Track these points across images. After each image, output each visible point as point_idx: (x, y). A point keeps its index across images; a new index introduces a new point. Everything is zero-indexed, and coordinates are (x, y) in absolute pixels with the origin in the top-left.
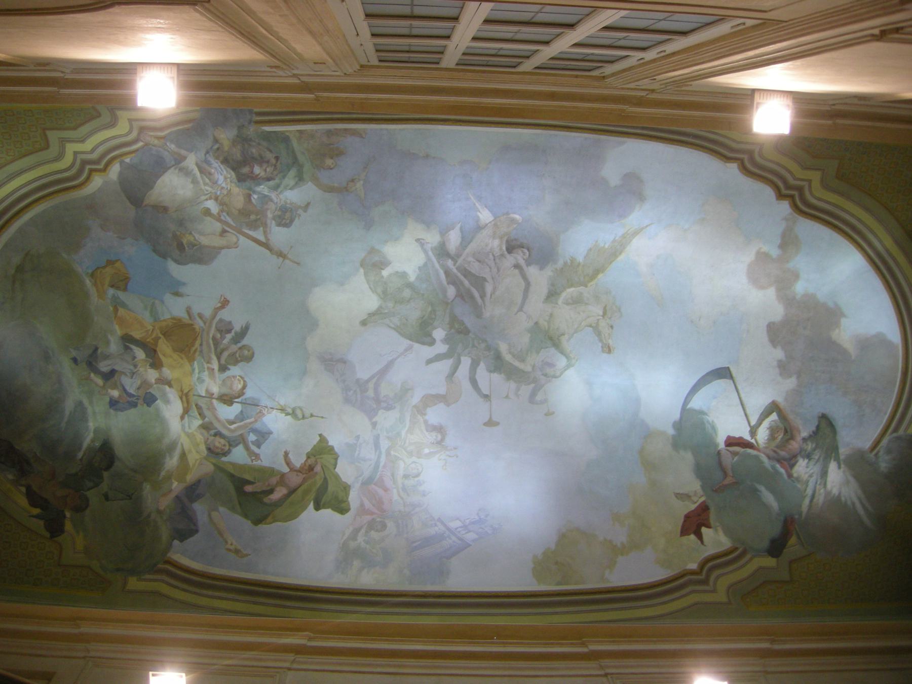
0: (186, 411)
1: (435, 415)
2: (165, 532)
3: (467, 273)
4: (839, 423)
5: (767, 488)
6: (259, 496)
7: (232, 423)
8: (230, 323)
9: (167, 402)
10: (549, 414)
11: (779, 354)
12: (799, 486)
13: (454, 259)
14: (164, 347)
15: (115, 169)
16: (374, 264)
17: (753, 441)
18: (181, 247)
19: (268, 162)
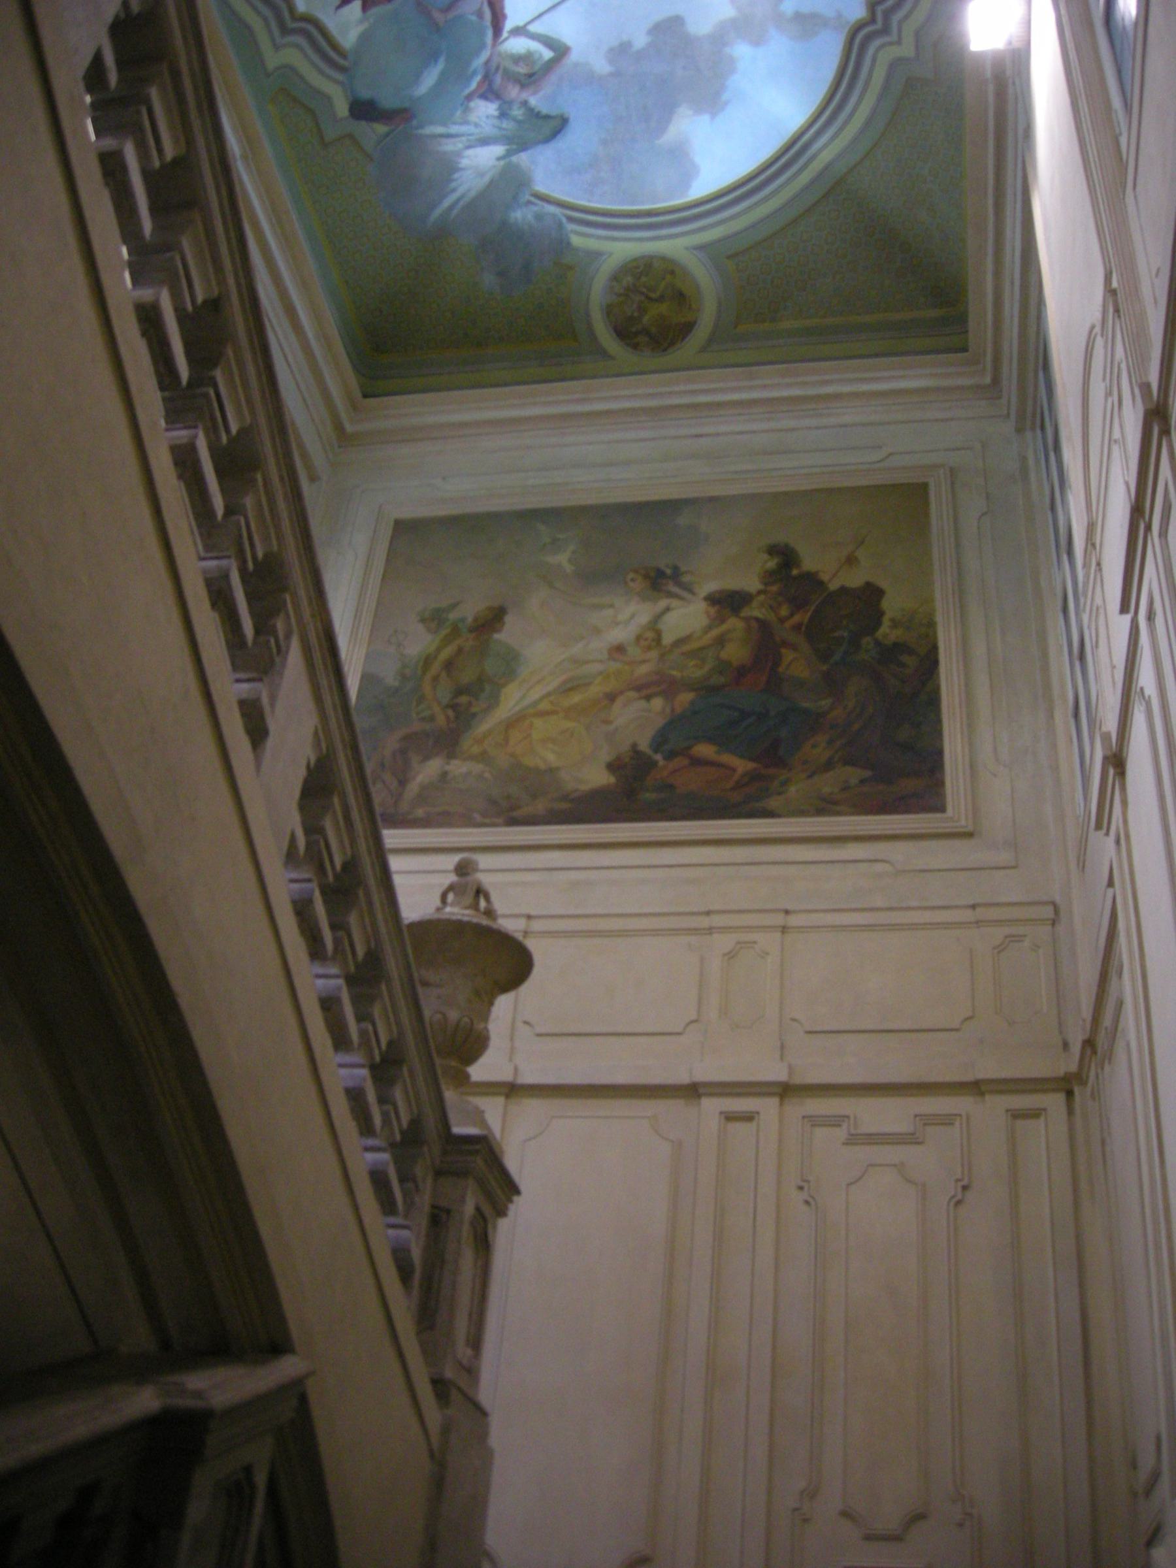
4: (563, 143)
5: (442, 73)
11: (640, 40)
12: (458, 113)
17: (505, 34)
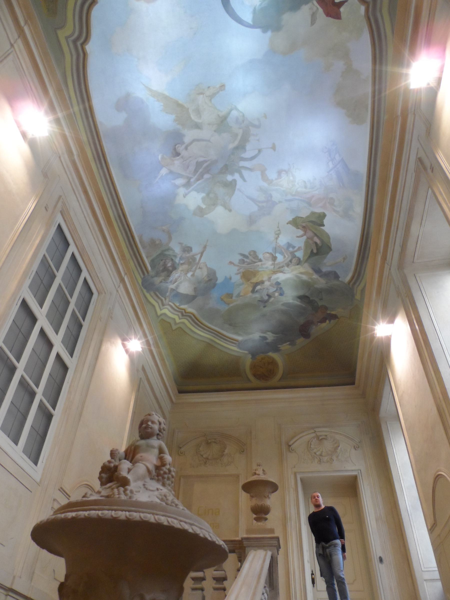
0: (282, 272)
1: (272, 175)
2: (336, 282)
3: (196, 171)
6: (319, 249)
7: (285, 257)
8: (239, 260)
9: (278, 278)
10: (265, 116)
13: (189, 179)
14: (254, 280)
15: (183, 307)
16: (200, 212)
18: (210, 280)
19: (165, 262)
